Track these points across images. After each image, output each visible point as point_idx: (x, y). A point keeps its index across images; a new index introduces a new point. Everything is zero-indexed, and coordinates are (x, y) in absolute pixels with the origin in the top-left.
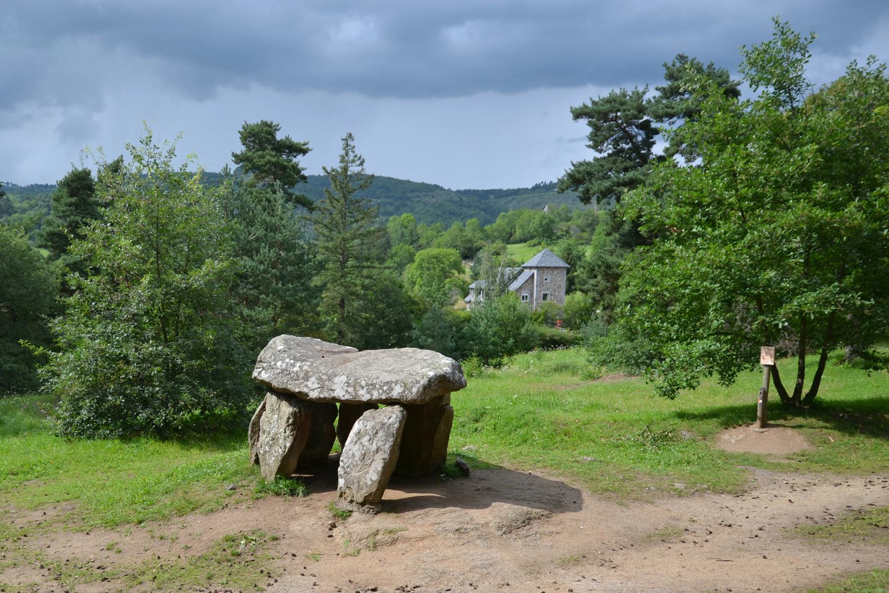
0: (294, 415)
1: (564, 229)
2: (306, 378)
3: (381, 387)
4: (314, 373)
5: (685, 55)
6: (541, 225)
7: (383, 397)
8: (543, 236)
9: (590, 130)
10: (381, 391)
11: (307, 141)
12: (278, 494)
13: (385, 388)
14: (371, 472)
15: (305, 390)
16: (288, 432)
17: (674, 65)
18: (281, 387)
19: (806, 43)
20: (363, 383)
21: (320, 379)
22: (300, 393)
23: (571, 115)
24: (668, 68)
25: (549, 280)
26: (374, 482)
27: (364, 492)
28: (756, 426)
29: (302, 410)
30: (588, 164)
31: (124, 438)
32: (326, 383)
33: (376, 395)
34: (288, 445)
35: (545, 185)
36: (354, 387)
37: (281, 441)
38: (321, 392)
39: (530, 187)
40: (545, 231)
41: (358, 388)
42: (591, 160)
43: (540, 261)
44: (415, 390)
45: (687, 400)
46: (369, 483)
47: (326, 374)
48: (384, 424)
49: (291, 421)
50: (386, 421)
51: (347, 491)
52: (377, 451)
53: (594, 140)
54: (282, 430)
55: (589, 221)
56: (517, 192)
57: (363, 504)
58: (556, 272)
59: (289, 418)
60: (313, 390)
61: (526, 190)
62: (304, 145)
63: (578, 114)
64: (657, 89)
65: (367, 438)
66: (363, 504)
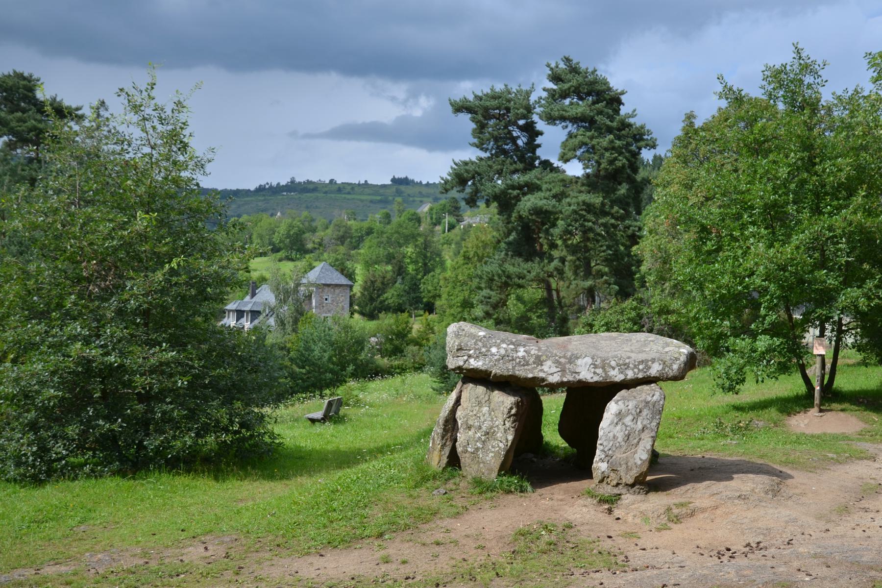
0: (517, 404)
1: (317, 240)
2: (539, 361)
3: (635, 366)
4: (548, 358)
5: (571, 58)
6: (288, 236)
7: (640, 376)
8: (291, 249)
9: (473, 126)
10: (636, 370)
11: (80, 105)
12: (509, 492)
13: (641, 367)
14: (639, 451)
15: (542, 375)
16: (508, 424)
17: (557, 67)
18: (506, 373)
19: (818, 68)
20: (613, 363)
21: (557, 363)
22: (534, 378)
23: (450, 108)
24: (552, 69)
25: (329, 301)
26: (644, 461)
27: (635, 473)
28: (814, 412)
29: (524, 399)
30: (473, 163)
31: (121, 473)
32: (567, 366)
33: (630, 375)
34: (510, 438)
35: (271, 187)
36: (603, 368)
37: (499, 435)
38: (563, 376)
39: (252, 189)
40: (293, 243)
41: (607, 369)
42: (474, 159)
43: (319, 277)
44: (675, 367)
45: (750, 392)
46: (639, 462)
47: (564, 357)
48: (648, 403)
49: (513, 411)
50: (649, 398)
51: (612, 474)
52: (643, 430)
53: (479, 138)
54: (500, 422)
55: (341, 233)
56: (237, 193)
57: (632, 486)
58: (337, 291)
59: (511, 408)
60: (552, 374)
61: (247, 192)
62: (78, 109)
63: (460, 108)
64: (544, 90)
65: (630, 417)
66: (632, 486)
